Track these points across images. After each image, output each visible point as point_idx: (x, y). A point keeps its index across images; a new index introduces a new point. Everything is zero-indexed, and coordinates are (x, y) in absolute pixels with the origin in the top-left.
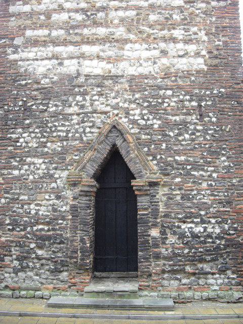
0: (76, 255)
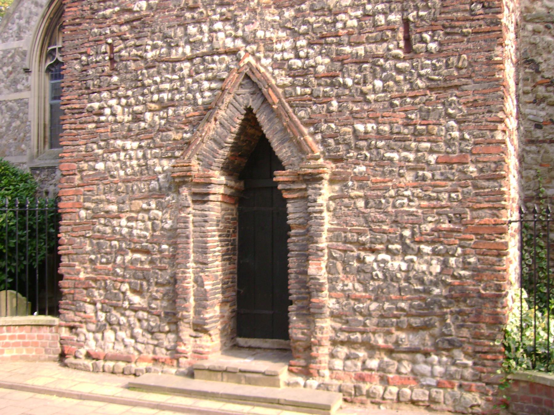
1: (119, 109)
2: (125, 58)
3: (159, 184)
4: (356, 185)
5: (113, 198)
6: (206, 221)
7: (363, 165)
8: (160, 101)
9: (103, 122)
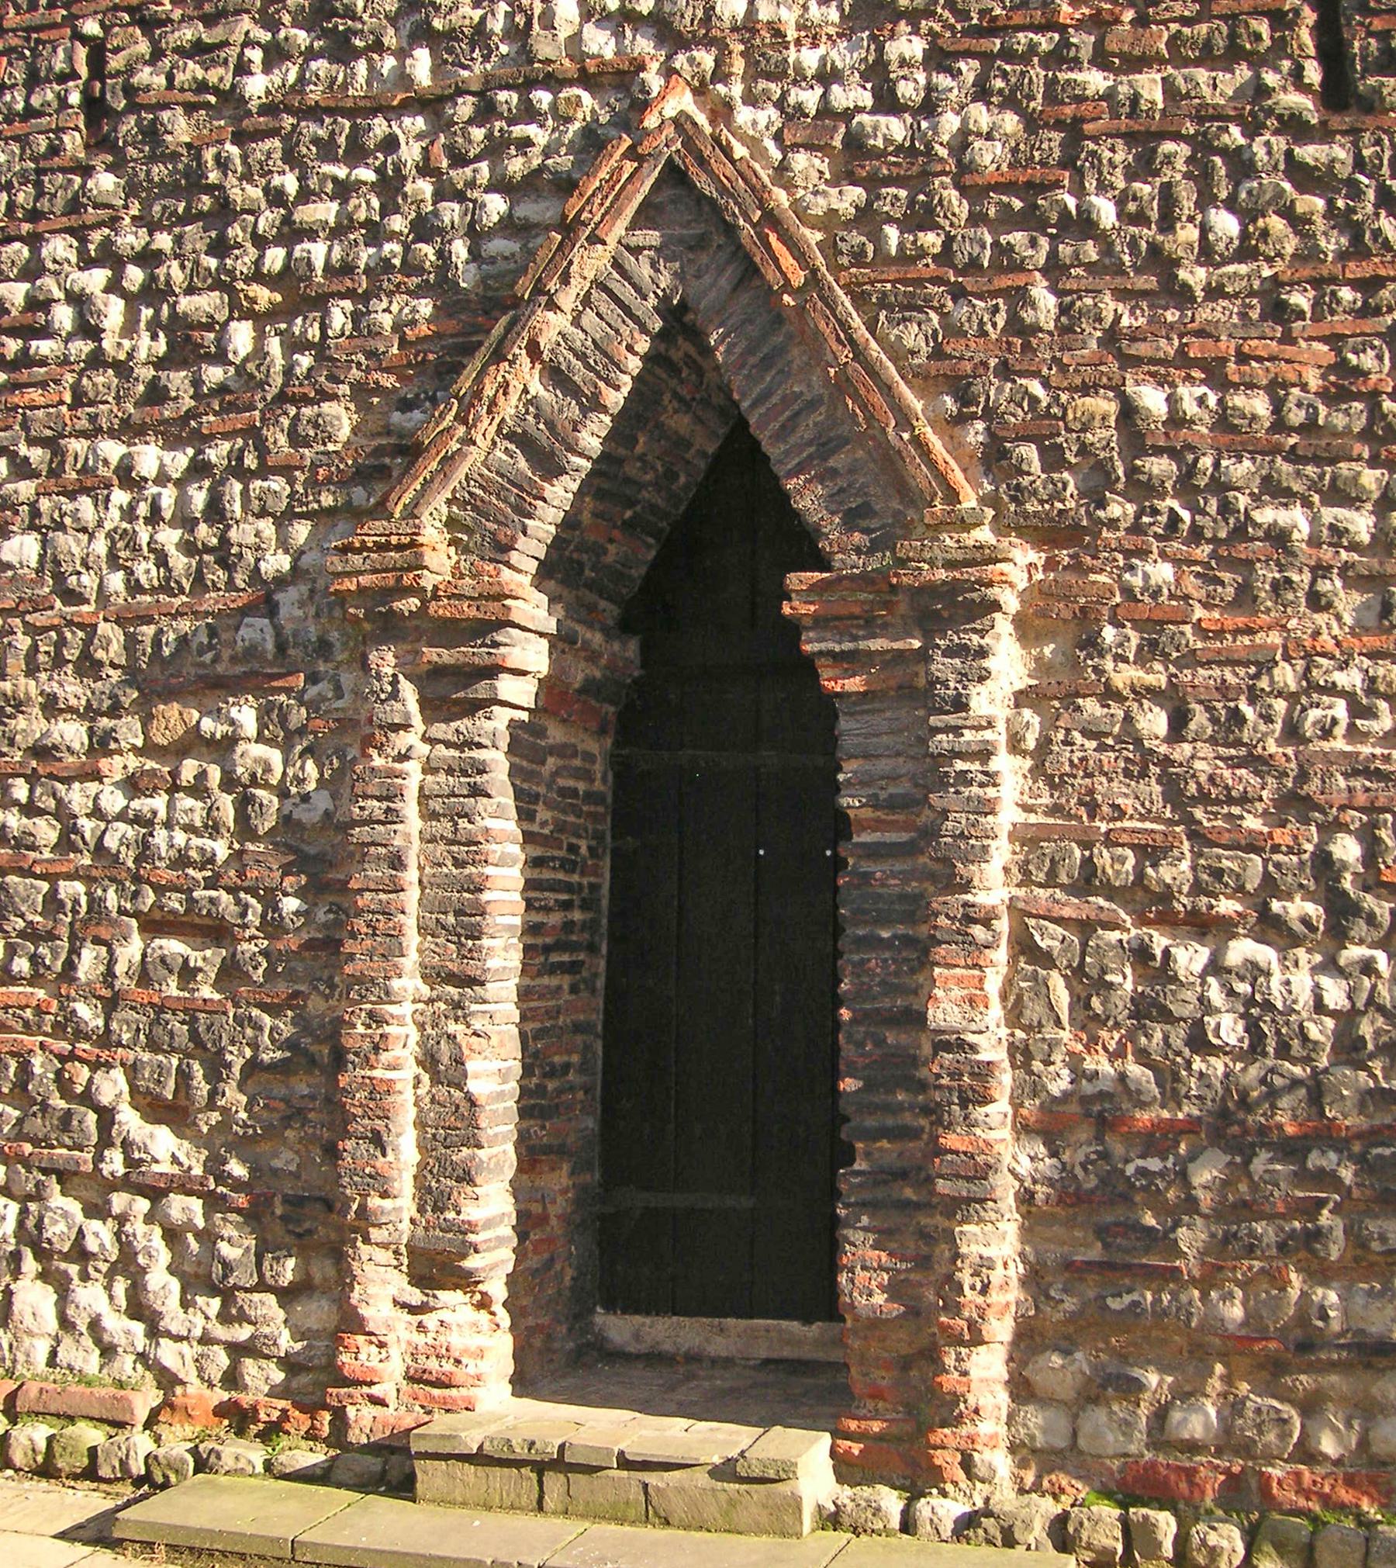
1: (114, 312)
2: (152, 98)
3: (278, 630)
4: (1135, 640)
5: (72, 689)
6: (477, 792)
7: (1163, 555)
8: (288, 278)
9: (43, 362)
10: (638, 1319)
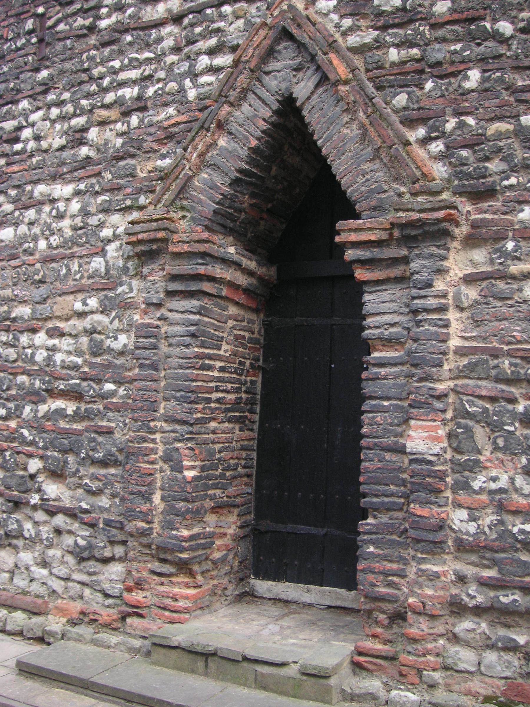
0: (145, 507)
3: (107, 262)
10: (270, 583)
